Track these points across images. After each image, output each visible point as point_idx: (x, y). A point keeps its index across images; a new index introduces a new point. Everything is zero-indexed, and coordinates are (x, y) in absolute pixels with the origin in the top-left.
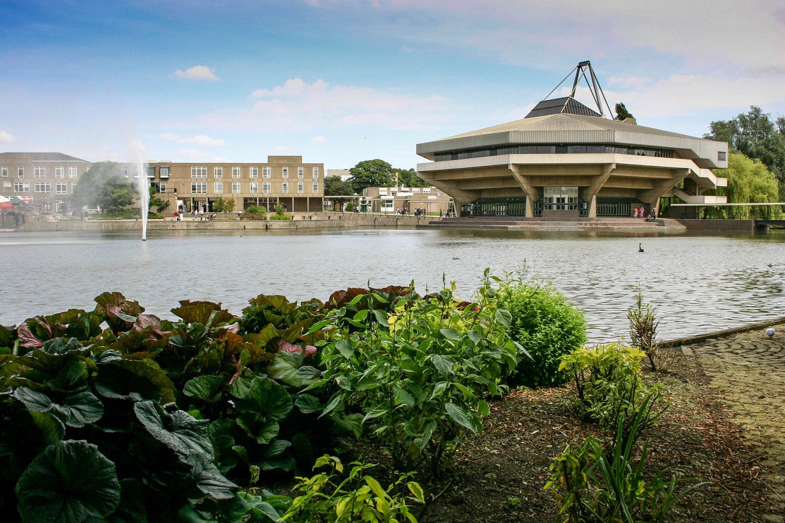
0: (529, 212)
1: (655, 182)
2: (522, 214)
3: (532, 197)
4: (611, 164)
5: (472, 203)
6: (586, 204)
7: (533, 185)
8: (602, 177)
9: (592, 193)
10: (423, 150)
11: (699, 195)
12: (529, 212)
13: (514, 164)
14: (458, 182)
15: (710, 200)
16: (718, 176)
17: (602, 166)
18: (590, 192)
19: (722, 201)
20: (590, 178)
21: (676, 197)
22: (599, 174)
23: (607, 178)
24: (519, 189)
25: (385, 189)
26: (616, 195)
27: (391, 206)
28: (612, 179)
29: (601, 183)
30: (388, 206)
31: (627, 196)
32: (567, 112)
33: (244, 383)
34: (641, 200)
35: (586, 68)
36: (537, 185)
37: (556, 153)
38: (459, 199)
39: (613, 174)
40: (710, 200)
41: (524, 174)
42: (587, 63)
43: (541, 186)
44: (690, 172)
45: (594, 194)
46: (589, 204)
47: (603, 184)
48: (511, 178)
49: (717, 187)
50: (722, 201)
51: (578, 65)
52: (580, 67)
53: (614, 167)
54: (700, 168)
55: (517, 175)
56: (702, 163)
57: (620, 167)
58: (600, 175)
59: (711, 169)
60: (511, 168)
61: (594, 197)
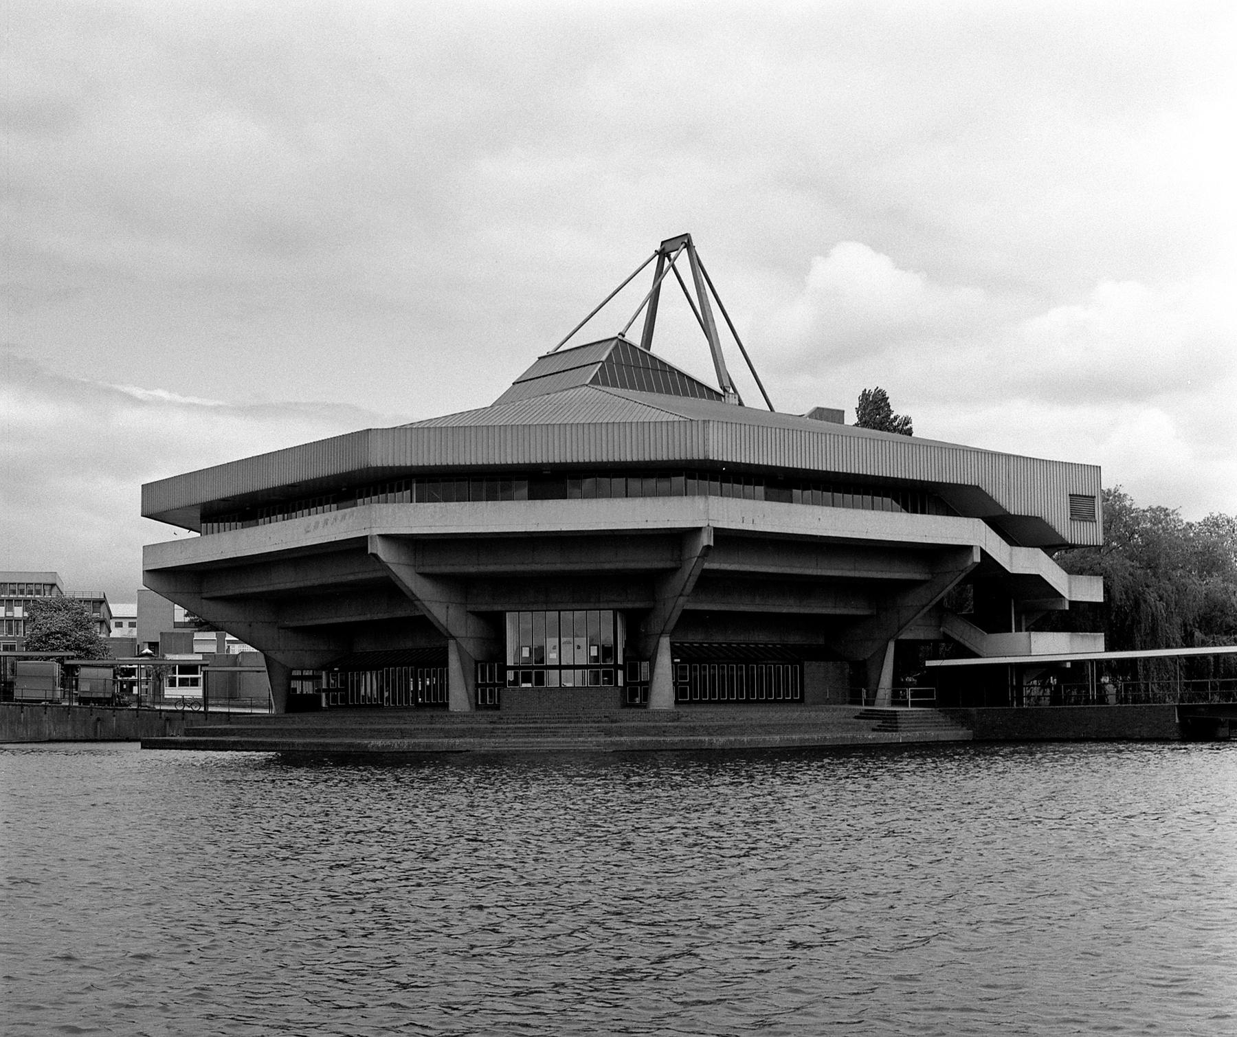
0: (459, 697)
1: (883, 595)
2: (438, 701)
3: (471, 647)
4: (700, 529)
5: (323, 668)
6: (645, 664)
7: (471, 608)
8: (679, 574)
9: (658, 630)
10: (160, 503)
11: (1019, 629)
12: (459, 697)
13: (385, 537)
14: (279, 602)
15: (1052, 646)
16: (1072, 569)
17: (678, 538)
18: (656, 627)
19: (1089, 647)
20: (651, 581)
21: (947, 639)
22: (669, 565)
23: (693, 580)
24: (425, 624)
25: (212, 635)
26: (761, 638)
27: (194, 683)
28: (709, 582)
29: (678, 598)
30: (183, 683)
31: (794, 639)
32: (605, 384)
33: (590, 909)
34: (974, 649)
35: (682, 260)
36: (484, 608)
37: (530, 498)
38: (279, 657)
39: (707, 566)
40: (1052, 646)
41: (428, 570)
42: (686, 241)
43: (498, 608)
44: (977, 558)
45: (662, 633)
46: (652, 660)
47: (682, 600)
48: (389, 589)
49: (1071, 603)
50: (1089, 647)
51: (658, 248)
52: (663, 253)
53: (706, 540)
54: (1011, 545)
55: (407, 576)
56: (1014, 529)
57: (727, 539)
58: (674, 571)
59: (1049, 549)
60: (378, 548)
61: (665, 642)
